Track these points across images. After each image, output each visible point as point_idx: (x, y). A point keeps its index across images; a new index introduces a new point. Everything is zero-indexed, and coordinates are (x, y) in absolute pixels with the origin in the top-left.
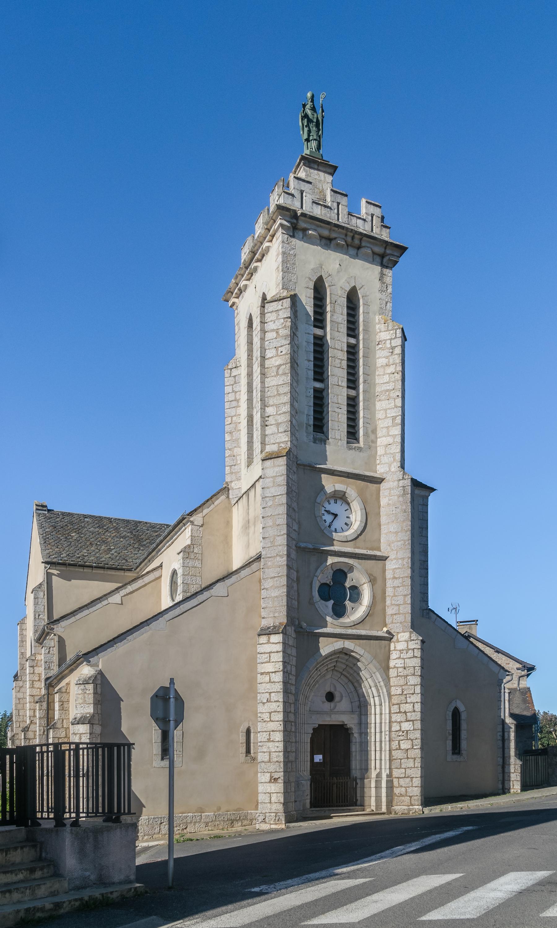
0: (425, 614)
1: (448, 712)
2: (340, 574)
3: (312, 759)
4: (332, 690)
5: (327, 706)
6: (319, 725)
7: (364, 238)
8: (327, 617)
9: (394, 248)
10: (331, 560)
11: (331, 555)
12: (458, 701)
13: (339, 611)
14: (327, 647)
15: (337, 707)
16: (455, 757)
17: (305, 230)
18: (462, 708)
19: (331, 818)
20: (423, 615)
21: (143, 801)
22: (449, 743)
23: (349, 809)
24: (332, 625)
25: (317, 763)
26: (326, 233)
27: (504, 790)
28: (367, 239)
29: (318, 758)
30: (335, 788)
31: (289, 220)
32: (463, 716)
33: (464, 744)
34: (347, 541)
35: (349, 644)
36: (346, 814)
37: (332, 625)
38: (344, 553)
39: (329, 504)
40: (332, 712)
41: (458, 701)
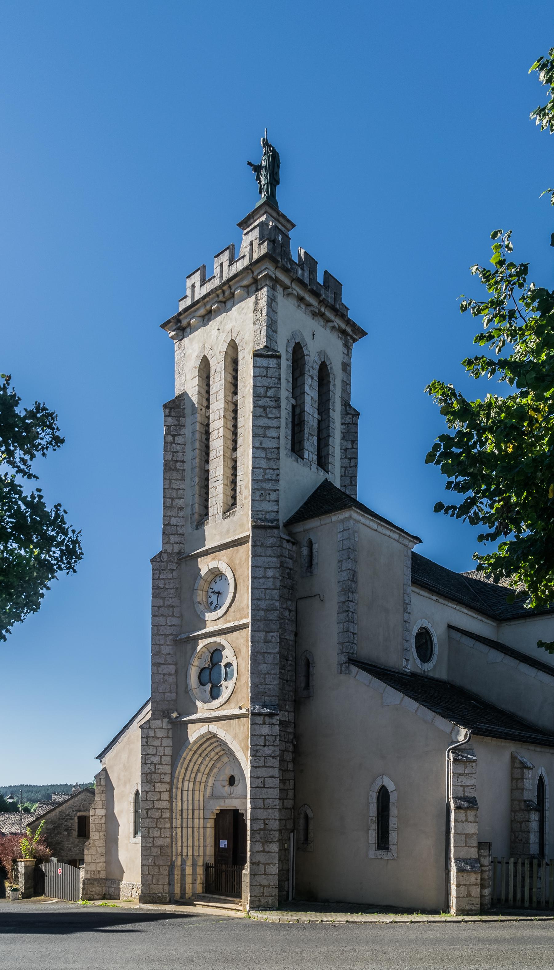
0: (343, 669)
1: (371, 793)
2: (216, 653)
3: (217, 844)
4: (233, 774)
5: (227, 789)
6: (221, 810)
7: (230, 283)
8: (197, 701)
9: (259, 264)
10: (202, 644)
11: (202, 638)
12: (384, 777)
13: (215, 694)
14: (195, 733)
15: (235, 792)
16: (380, 853)
17: (189, 324)
18: (391, 787)
19: (195, 905)
20: (341, 670)
21: (125, 869)
22: (373, 836)
23: (230, 900)
24: (203, 709)
25: (222, 848)
26: (202, 311)
27: (446, 909)
28: (233, 281)
29: (223, 844)
30: (224, 876)
31: (174, 328)
32: (393, 798)
33: (393, 837)
34: (219, 619)
35: (213, 728)
36: (205, 904)
37: (203, 709)
38: (212, 632)
39: (221, 580)
40: (230, 796)
41: (384, 777)
